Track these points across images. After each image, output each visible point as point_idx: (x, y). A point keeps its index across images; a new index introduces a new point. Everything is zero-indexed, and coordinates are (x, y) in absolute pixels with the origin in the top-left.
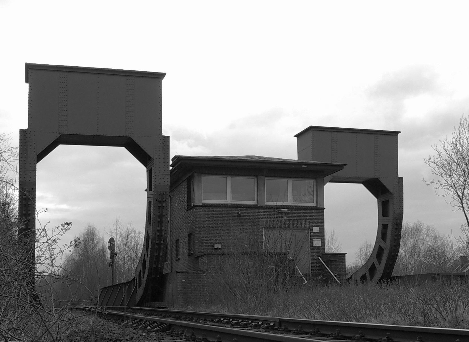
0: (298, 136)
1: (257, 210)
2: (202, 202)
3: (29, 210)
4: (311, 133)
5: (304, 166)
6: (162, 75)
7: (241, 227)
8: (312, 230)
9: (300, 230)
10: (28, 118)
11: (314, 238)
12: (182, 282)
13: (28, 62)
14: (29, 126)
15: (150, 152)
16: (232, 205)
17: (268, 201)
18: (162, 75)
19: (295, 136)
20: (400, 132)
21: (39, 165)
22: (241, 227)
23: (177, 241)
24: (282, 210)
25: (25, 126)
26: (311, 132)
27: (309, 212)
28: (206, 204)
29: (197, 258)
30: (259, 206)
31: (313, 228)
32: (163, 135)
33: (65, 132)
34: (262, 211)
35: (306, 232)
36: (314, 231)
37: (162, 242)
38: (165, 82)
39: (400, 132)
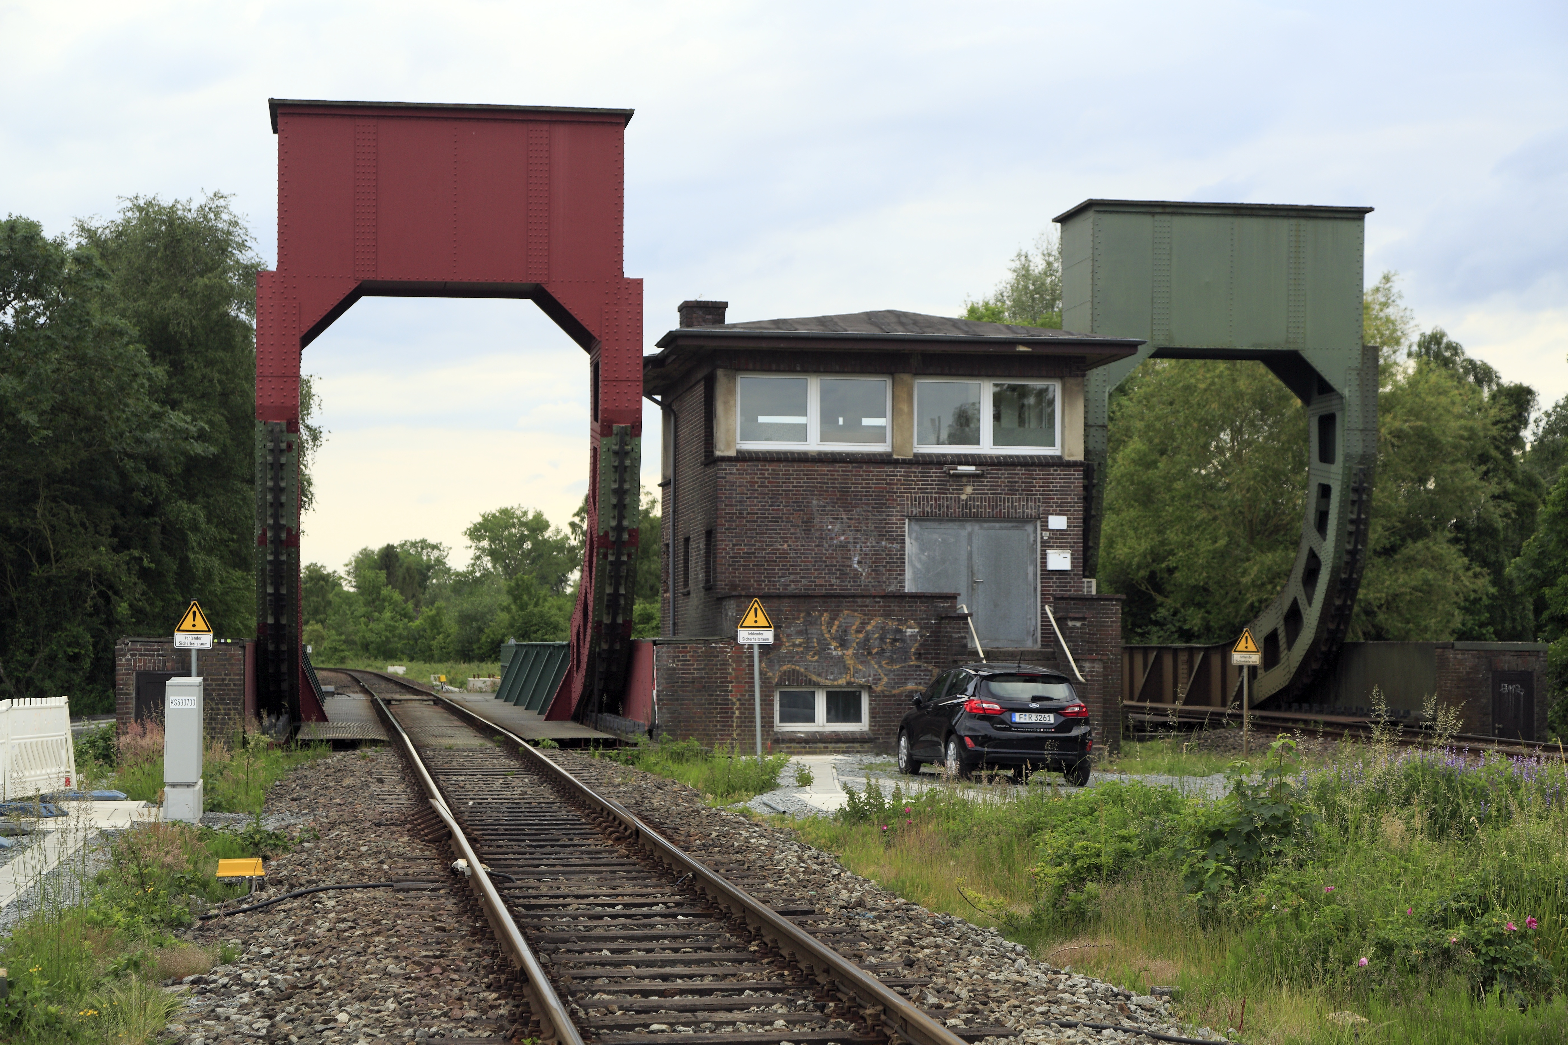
0: (1064, 219)
1: (888, 469)
2: (738, 447)
3: (282, 479)
4: (1091, 220)
5: (1022, 349)
6: (625, 116)
8: (1045, 527)
9: (1010, 525)
10: (277, 183)
11: (1051, 547)
12: (669, 669)
13: (276, 97)
15: (591, 327)
16: (820, 454)
17: (920, 442)
18: (625, 116)
19: (1056, 220)
20: (1371, 210)
21: (304, 352)
22: (844, 517)
23: (687, 540)
24: (959, 468)
26: (1090, 217)
29: (720, 600)
30: (895, 457)
31: (1050, 517)
32: (626, 276)
34: (901, 471)
35: (1029, 528)
36: (1050, 527)
37: (624, 558)
38: (631, 132)
39: (1371, 210)
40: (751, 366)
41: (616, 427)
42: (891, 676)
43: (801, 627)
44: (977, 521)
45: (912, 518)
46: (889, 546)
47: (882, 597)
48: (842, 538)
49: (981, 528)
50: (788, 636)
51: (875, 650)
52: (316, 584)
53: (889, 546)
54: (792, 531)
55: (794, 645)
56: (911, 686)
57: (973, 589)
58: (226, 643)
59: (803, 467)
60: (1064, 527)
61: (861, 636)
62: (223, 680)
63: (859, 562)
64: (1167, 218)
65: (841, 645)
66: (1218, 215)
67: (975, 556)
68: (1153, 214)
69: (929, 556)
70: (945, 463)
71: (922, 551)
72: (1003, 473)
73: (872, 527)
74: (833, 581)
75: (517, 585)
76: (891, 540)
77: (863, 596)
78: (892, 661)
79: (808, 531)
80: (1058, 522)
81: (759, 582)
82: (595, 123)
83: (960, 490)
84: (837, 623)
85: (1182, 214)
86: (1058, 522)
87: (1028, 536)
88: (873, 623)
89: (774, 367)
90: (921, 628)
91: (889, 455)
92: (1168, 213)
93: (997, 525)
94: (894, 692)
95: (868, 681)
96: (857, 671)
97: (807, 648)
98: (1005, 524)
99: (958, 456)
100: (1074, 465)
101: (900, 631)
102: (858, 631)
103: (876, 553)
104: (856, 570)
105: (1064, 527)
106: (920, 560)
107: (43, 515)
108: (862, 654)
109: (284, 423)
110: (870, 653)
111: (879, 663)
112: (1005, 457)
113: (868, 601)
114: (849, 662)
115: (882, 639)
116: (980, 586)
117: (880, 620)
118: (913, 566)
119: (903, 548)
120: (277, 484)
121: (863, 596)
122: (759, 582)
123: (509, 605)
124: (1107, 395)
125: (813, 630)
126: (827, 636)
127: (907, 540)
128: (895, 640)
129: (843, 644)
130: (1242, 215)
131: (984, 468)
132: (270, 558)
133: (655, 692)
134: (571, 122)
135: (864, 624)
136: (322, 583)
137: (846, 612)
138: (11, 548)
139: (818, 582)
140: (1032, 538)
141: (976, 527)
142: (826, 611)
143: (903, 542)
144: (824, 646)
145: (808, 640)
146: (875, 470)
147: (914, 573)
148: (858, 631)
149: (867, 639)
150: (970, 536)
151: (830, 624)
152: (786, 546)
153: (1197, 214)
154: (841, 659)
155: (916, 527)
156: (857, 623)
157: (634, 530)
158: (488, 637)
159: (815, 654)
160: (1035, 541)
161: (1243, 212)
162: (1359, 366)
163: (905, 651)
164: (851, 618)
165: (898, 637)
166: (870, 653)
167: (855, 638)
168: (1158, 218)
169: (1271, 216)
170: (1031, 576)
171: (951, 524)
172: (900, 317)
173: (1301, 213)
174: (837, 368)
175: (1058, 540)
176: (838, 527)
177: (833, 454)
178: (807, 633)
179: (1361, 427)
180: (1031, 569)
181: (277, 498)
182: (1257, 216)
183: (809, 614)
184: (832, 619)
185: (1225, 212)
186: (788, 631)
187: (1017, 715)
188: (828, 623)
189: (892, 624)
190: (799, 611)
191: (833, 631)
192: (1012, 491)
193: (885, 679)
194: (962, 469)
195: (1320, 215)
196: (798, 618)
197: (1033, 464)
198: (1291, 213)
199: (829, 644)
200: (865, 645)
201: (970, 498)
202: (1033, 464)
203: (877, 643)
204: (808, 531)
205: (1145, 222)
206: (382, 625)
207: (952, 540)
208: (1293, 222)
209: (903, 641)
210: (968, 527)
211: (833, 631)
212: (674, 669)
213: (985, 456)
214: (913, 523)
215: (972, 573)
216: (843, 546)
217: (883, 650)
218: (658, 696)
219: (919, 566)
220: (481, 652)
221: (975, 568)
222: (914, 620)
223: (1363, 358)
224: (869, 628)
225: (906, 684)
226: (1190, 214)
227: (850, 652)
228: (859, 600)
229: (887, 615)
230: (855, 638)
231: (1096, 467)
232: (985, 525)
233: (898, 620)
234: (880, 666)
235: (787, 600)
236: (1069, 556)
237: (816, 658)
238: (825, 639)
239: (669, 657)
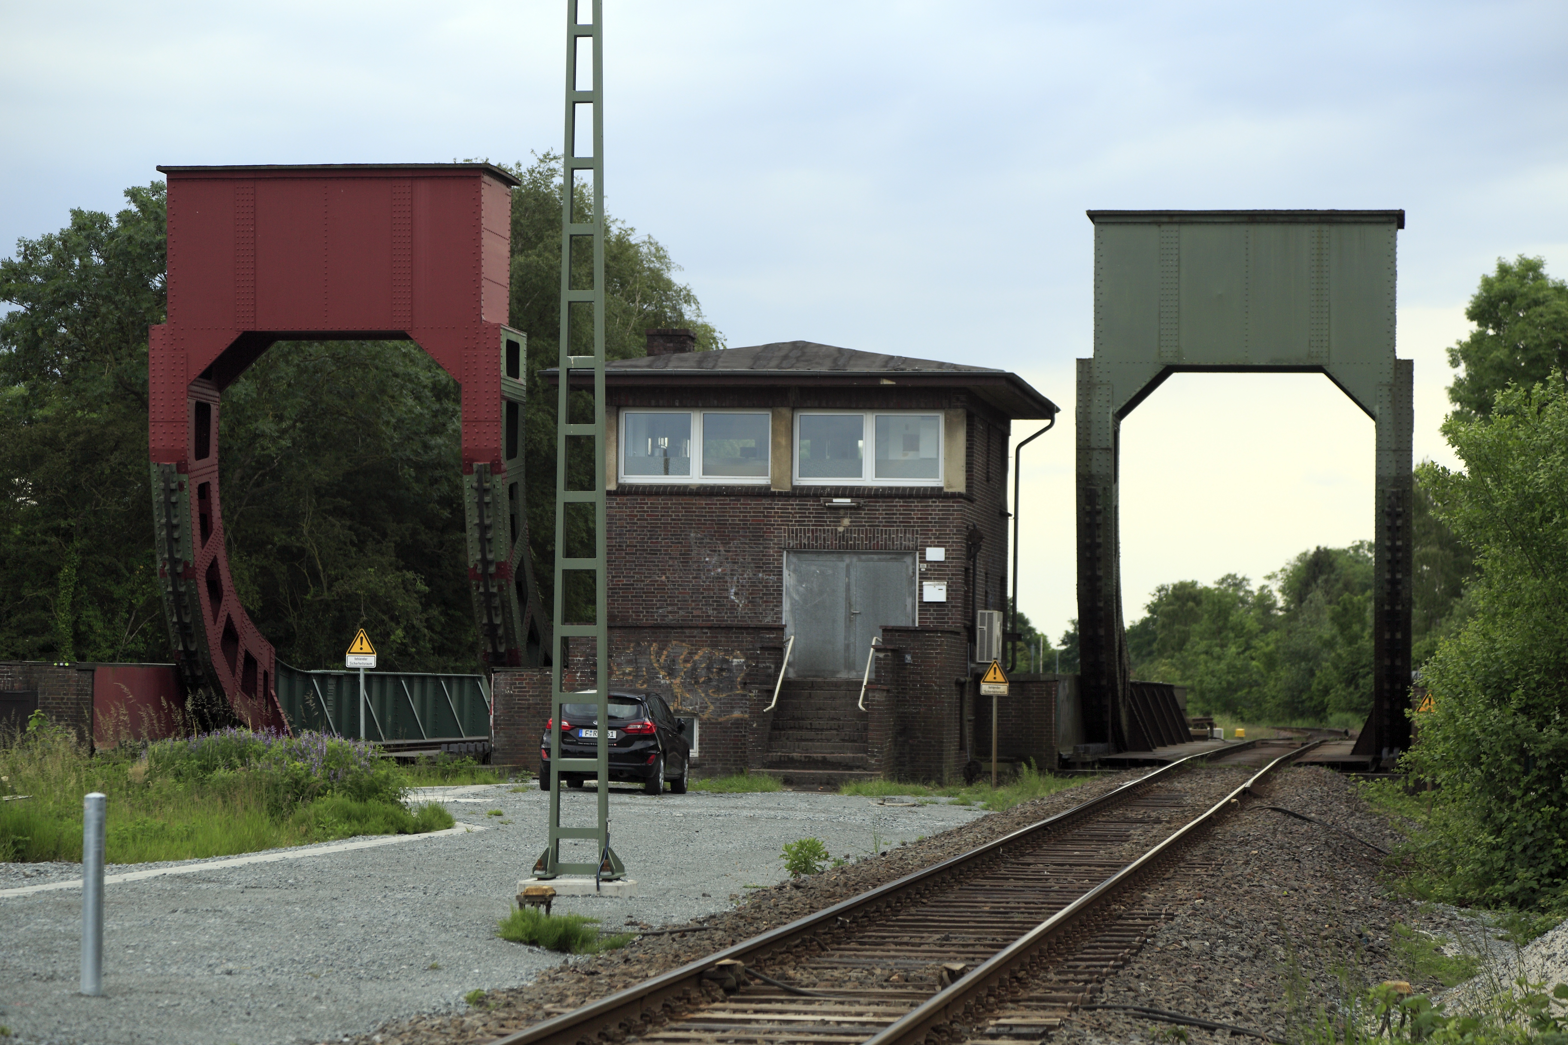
1: (766, 502)
6: (1397, 219)
7: (722, 549)
8: (923, 560)
9: (889, 557)
12: (506, 695)
14: (1096, 349)
18: (1397, 219)
22: (722, 549)
24: (835, 500)
25: (1088, 353)
27: (916, 504)
28: (637, 487)
30: (772, 490)
33: (251, 328)
35: (908, 560)
36: (928, 559)
40: (631, 402)
41: (475, 465)
42: (718, 704)
43: (632, 656)
44: (855, 553)
45: (791, 550)
46: (766, 577)
47: (709, 628)
48: (720, 570)
49: (860, 560)
50: (618, 665)
51: (703, 679)
52: (1184, 604)
53: (766, 577)
54: (671, 563)
55: (624, 674)
56: (737, 714)
57: (850, 621)
58: (64, 666)
59: (681, 500)
60: (942, 559)
61: (689, 665)
62: (62, 699)
63: (736, 594)
64: (1175, 227)
65: (669, 674)
66: (1231, 223)
67: (853, 588)
68: (1159, 224)
69: (806, 588)
70: (821, 495)
71: (800, 582)
72: (881, 505)
73: (749, 559)
74: (710, 612)
75: (1345, 609)
76: (768, 572)
77: (691, 627)
78: (718, 690)
79: (685, 563)
80: (936, 554)
81: (637, 613)
82: (454, 177)
83: (838, 522)
84: (665, 652)
85: (1192, 223)
86: (936, 554)
87: (907, 567)
88: (700, 653)
89: (653, 402)
90: (747, 658)
91: (767, 487)
92: (1176, 223)
93: (875, 557)
94: (720, 720)
95: (695, 709)
96: (684, 699)
97: (636, 676)
98: (884, 556)
99: (838, 488)
100: (954, 496)
101: (727, 661)
102: (686, 661)
103: (753, 585)
104: (733, 601)
105: (942, 559)
106: (798, 592)
107: (311, 532)
108: (690, 683)
109: (174, 464)
110: (697, 682)
111: (706, 692)
112: (884, 488)
113: (695, 632)
114: (677, 691)
115: (709, 668)
116: (858, 618)
117: (707, 650)
118: (792, 598)
119: (780, 580)
120: (169, 521)
121: (691, 627)
122: (637, 613)
123: (1334, 637)
124: (1110, 416)
125: (642, 660)
126: (656, 665)
127: (785, 573)
128: (721, 670)
129: (671, 673)
130: (1258, 222)
131: (862, 501)
132: (170, 589)
133: (492, 717)
134: (431, 177)
135: (691, 654)
136: (1191, 604)
137: (674, 643)
138: (284, 568)
139: (695, 613)
140: (911, 571)
141: (855, 559)
142: (655, 641)
143: (780, 574)
144: (653, 675)
145: (638, 669)
146: (753, 503)
147: (792, 604)
148: (686, 661)
149: (694, 669)
150: (848, 567)
151: (659, 654)
152: (664, 578)
153: (1207, 223)
154: (669, 688)
155: (794, 559)
156: (685, 653)
157: (501, 563)
158: (1319, 683)
159: (644, 682)
160: (914, 573)
161: (1258, 218)
162: (1392, 381)
163: (731, 680)
164: (679, 649)
165: (725, 666)
166: (697, 682)
167: (683, 667)
168: (1164, 227)
169: (1290, 222)
170: (909, 607)
171: (829, 557)
172: (800, 349)
173: (1323, 218)
174: (716, 402)
175: (935, 572)
176: (715, 559)
177: (713, 487)
178: (636, 663)
179: (1394, 447)
180: (909, 601)
181: (169, 534)
182: (1275, 222)
183: (639, 644)
184: (661, 649)
185: (1238, 219)
186: (619, 660)
187: (584, 731)
188: (657, 653)
189: (719, 655)
190: (630, 641)
191: (662, 661)
192: (890, 523)
193: (712, 707)
194: (837, 501)
195: (1344, 219)
196: (628, 648)
197: (910, 496)
198: (1312, 219)
199: (658, 673)
200: (693, 674)
201: (847, 530)
202: (910, 496)
203: (704, 672)
204: (685, 563)
205: (1153, 232)
206: (1223, 665)
207: (830, 572)
208: (1315, 227)
209: (729, 670)
210: (847, 559)
211: (662, 661)
212: (511, 695)
213: (864, 488)
214: (791, 556)
215: (849, 604)
216: (720, 578)
217: (710, 680)
218: (495, 720)
219: (797, 597)
220: (1313, 703)
221: (853, 599)
222: (741, 650)
223: (1395, 373)
224: (696, 657)
225: (732, 712)
226: (1200, 223)
227: (678, 681)
228: (687, 631)
229: (714, 645)
230: (683, 667)
231: (1100, 493)
232: (863, 557)
233: (725, 651)
234: (707, 695)
235: (618, 631)
236: (944, 588)
237: (645, 686)
238: (654, 669)
239: (506, 684)
